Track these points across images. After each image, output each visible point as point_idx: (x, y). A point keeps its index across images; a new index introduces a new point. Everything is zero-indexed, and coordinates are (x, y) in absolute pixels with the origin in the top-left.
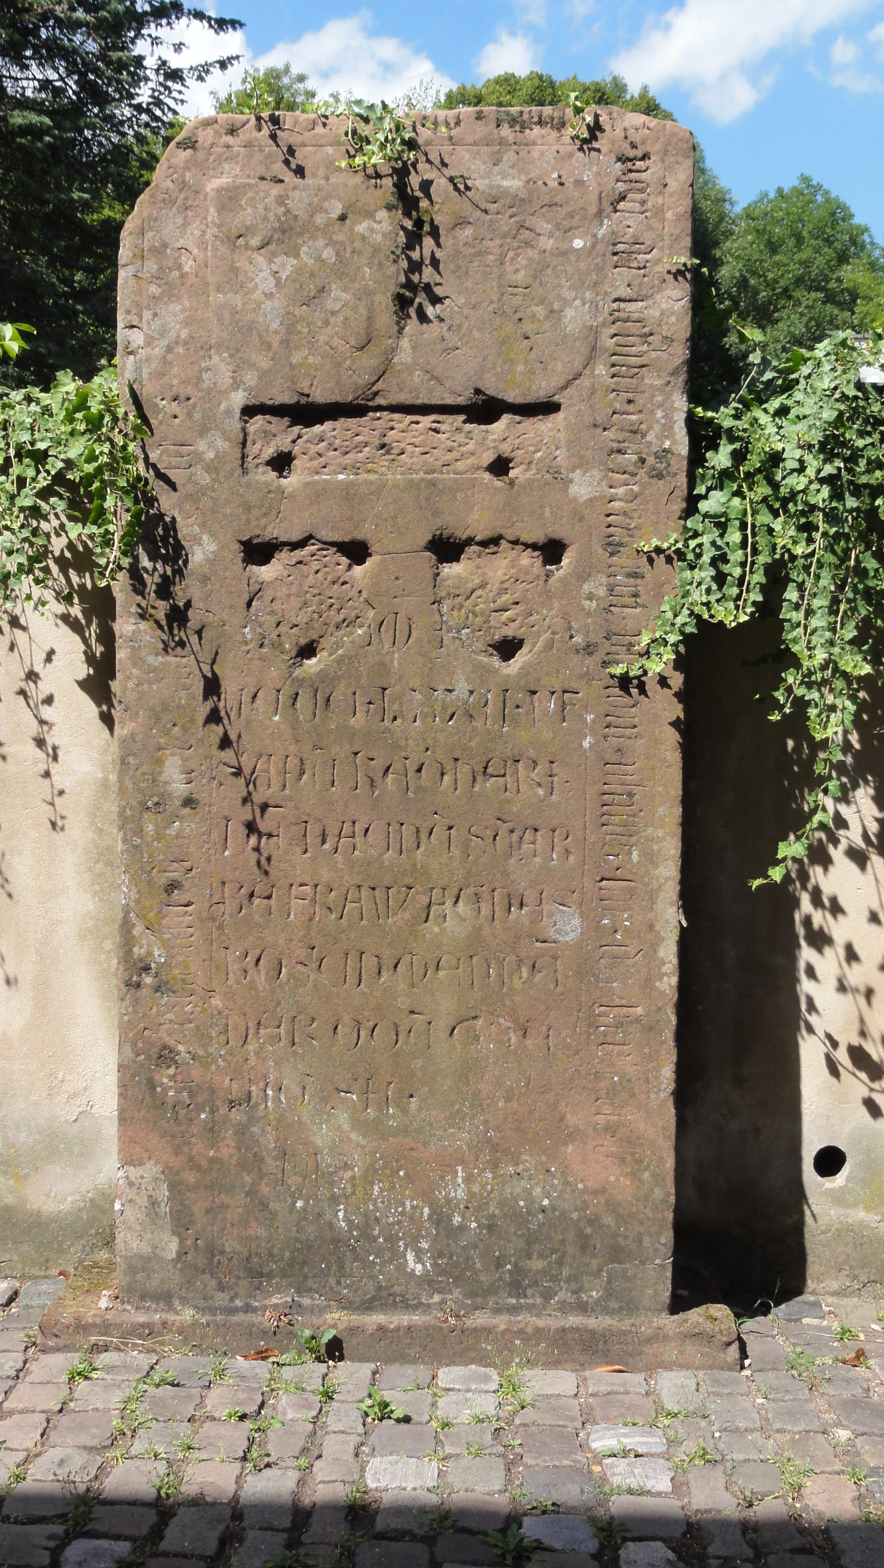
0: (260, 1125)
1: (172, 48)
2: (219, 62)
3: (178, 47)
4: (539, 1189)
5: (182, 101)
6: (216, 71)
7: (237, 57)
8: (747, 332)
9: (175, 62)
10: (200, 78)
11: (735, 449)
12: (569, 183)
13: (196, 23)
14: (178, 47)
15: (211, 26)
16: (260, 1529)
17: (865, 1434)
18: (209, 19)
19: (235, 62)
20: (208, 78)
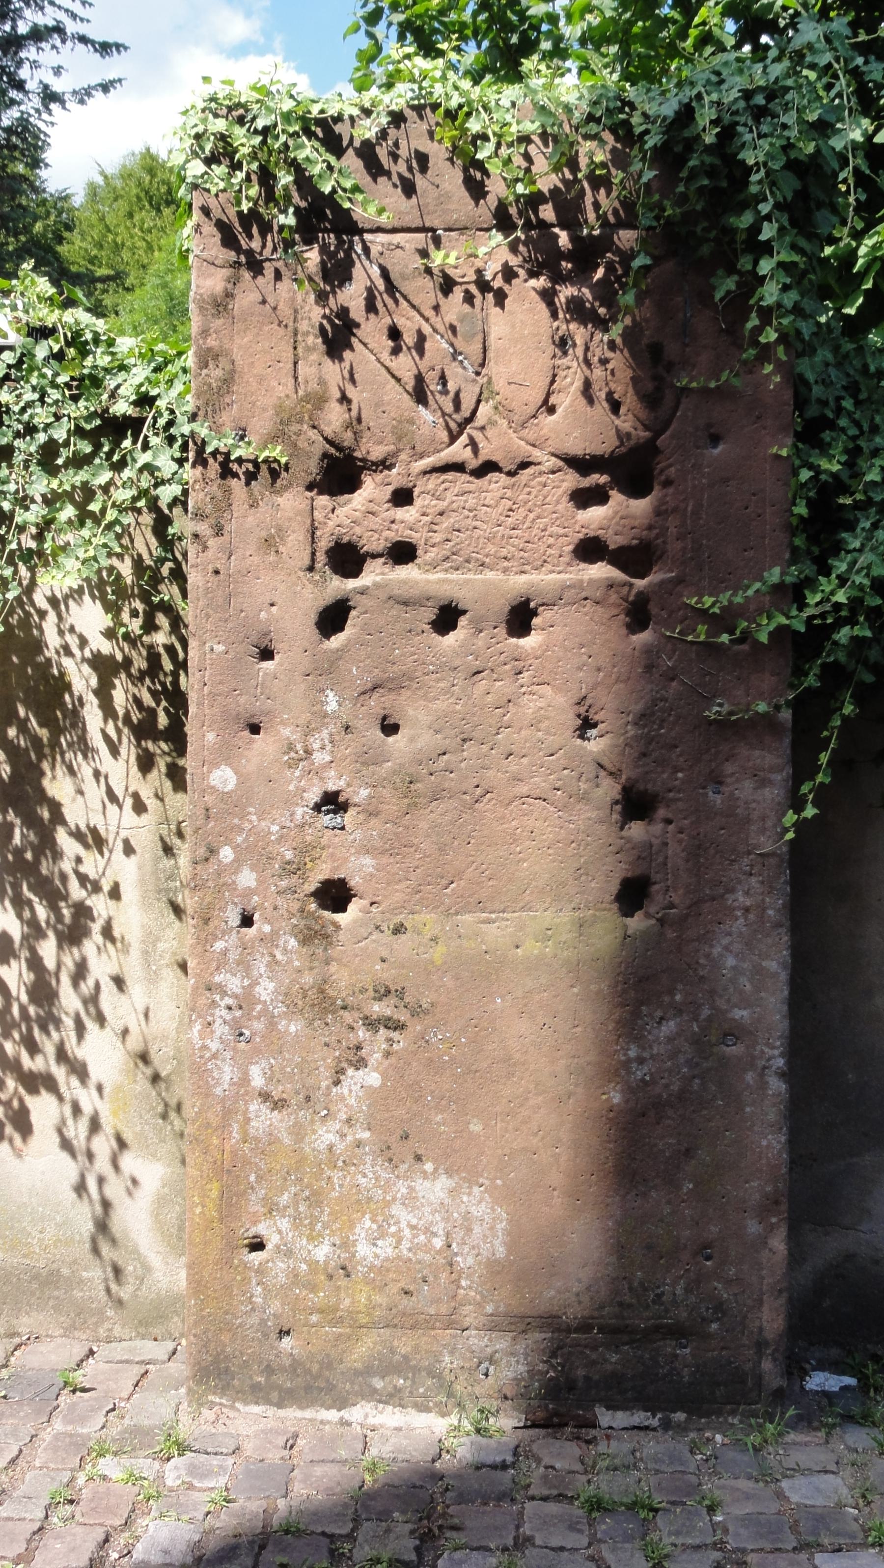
0: (834, 434)
1: (51, 72)
2: (101, 85)
3: (57, 71)
4: (530, 706)
5: (52, 124)
6: (99, 95)
7: (120, 80)
8: (185, 235)
9: (58, 85)
10: (82, 102)
11: (626, 328)
12: (178, 137)
13: (80, 47)
14: (57, 71)
15: (96, 50)
16: (24, 1519)
17: (20, 1345)
18: (93, 43)
19: (118, 85)
20: (90, 102)
